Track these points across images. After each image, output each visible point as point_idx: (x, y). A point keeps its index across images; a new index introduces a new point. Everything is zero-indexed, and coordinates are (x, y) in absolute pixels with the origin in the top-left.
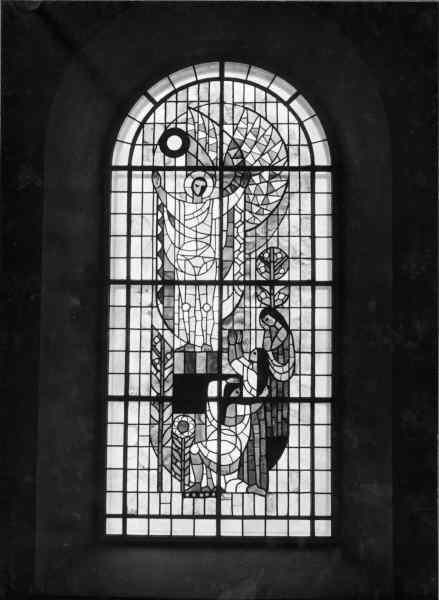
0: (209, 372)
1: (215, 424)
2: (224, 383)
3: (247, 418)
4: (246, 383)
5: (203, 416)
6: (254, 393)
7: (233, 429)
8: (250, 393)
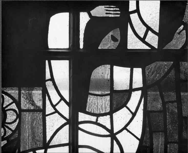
0: (32, 148)
1: (64, 109)
2: (84, 18)
3: (136, 96)
4: (134, 17)
5: (37, 94)
6: (153, 40)
7: (106, 121)
8: (143, 40)
